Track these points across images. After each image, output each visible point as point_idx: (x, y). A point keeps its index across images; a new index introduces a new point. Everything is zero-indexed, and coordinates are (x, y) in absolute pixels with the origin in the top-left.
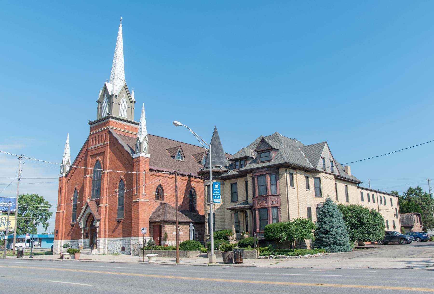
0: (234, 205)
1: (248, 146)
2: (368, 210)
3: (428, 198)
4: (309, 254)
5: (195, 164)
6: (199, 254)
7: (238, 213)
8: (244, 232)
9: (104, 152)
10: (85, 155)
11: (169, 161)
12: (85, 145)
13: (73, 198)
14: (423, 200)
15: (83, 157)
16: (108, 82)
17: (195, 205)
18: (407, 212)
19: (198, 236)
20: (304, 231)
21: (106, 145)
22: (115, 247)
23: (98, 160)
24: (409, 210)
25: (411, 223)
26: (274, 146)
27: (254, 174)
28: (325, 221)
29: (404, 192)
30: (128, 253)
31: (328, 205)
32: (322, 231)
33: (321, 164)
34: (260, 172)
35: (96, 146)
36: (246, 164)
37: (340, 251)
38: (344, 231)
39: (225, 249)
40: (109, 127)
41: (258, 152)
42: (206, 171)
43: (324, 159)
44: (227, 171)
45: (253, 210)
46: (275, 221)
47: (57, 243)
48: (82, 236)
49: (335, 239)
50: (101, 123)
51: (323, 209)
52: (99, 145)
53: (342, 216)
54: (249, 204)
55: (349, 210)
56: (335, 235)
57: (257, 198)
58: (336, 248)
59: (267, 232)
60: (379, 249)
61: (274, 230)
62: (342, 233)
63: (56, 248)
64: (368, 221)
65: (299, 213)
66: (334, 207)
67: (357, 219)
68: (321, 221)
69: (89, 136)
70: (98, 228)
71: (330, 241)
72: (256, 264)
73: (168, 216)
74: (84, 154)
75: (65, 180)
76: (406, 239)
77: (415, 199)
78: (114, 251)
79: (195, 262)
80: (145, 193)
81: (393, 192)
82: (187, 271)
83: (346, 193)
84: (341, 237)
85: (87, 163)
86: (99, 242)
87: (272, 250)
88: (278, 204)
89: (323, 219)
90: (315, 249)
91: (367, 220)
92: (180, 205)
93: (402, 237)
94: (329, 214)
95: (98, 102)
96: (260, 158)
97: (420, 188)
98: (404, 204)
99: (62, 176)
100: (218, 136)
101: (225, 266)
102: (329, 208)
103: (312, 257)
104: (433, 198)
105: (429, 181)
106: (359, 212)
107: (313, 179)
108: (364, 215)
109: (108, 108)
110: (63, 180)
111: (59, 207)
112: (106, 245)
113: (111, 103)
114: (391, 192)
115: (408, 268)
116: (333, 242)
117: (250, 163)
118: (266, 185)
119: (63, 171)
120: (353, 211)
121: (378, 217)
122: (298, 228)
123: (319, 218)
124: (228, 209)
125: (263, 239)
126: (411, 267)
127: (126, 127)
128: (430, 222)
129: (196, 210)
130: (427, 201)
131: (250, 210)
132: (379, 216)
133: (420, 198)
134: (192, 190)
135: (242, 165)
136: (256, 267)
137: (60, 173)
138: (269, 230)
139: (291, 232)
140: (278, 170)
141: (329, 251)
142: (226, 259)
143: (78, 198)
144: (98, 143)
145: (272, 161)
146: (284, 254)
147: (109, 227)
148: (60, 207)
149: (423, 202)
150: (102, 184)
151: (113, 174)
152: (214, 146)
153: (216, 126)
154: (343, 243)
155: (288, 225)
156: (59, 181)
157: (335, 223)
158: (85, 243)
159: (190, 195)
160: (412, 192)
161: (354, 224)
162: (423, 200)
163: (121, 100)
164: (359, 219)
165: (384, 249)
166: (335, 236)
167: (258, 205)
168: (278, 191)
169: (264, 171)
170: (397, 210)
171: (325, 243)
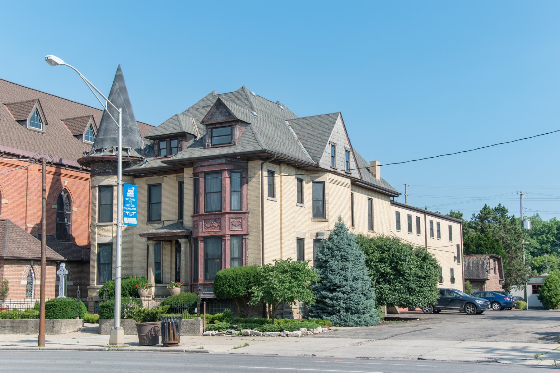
0: (153, 228)
1: (185, 111)
2: (411, 248)
3: (516, 228)
4: (303, 329)
5: (70, 140)
6: (81, 326)
7: (160, 243)
8: (173, 283)
11: (14, 130)
14: (508, 232)
17: (69, 225)
18: (477, 253)
19: (80, 290)
20: (295, 284)
24: (481, 249)
25: (483, 273)
26: (240, 117)
27: (198, 168)
28: (331, 267)
29: (474, 215)
31: (340, 235)
32: (325, 285)
33: (328, 155)
34: (210, 165)
36: (181, 149)
37: (357, 323)
38: (366, 286)
39: (144, 317)
41: (207, 125)
42: (97, 157)
43: (335, 146)
44: (141, 160)
45: (192, 241)
46: (236, 264)
49: (349, 300)
51: (331, 245)
53: (364, 257)
54: (184, 228)
55: (376, 246)
56: (349, 293)
57: (202, 217)
58: (350, 318)
59: (221, 285)
60: (428, 322)
61: (233, 280)
62: (363, 291)
64: (411, 269)
65: (281, 249)
66: (350, 240)
67: (390, 265)
68: (324, 267)
71: (339, 305)
72: (206, 348)
76: (475, 305)
77: (492, 229)
79: (78, 342)
81: (452, 214)
82: (79, 362)
83: (370, 214)
84: (360, 298)
87: (230, 320)
88: (244, 229)
89: (329, 262)
90: (310, 318)
91: (409, 268)
92: (37, 224)
93: (468, 301)
94: (340, 253)
96: (212, 137)
97: (503, 207)
98: (472, 238)
100: (125, 85)
101: (145, 350)
102: (341, 241)
103: (307, 335)
104: (526, 228)
105: (522, 195)
106: (395, 251)
107: (311, 183)
108: (403, 257)
114: (449, 214)
115: (489, 362)
116: (344, 306)
117: (191, 146)
118: (221, 192)
120: (384, 250)
121: (429, 262)
122: (285, 279)
123: (321, 260)
124: (141, 235)
125: (211, 297)
126: (496, 359)
128: (518, 272)
129: (71, 235)
130: (515, 233)
131: (186, 240)
132: (431, 260)
133: (503, 227)
134: (63, 193)
135: (173, 149)
136: (207, 352)
138: (225, 280)
139: (271, 285)
140: (246, 164)
141: (337, 323)
142: (145, 337)
145: (235, 145)
146: (255, 329)
149: (506, 235)
153: (119, 65)
154: (364, 309)
155: (263, 272)
157: (350, 270)
159: (57, 204)
160: (488, 216)
161: (384, 273)
162: (508, 231)
164: (394, 264)
165: (436, 322)
166: (349, 296)
167: (203, 231)
168: (244, 204)
169: (219, 164)
170: (460, 249)
171: (330, 309)
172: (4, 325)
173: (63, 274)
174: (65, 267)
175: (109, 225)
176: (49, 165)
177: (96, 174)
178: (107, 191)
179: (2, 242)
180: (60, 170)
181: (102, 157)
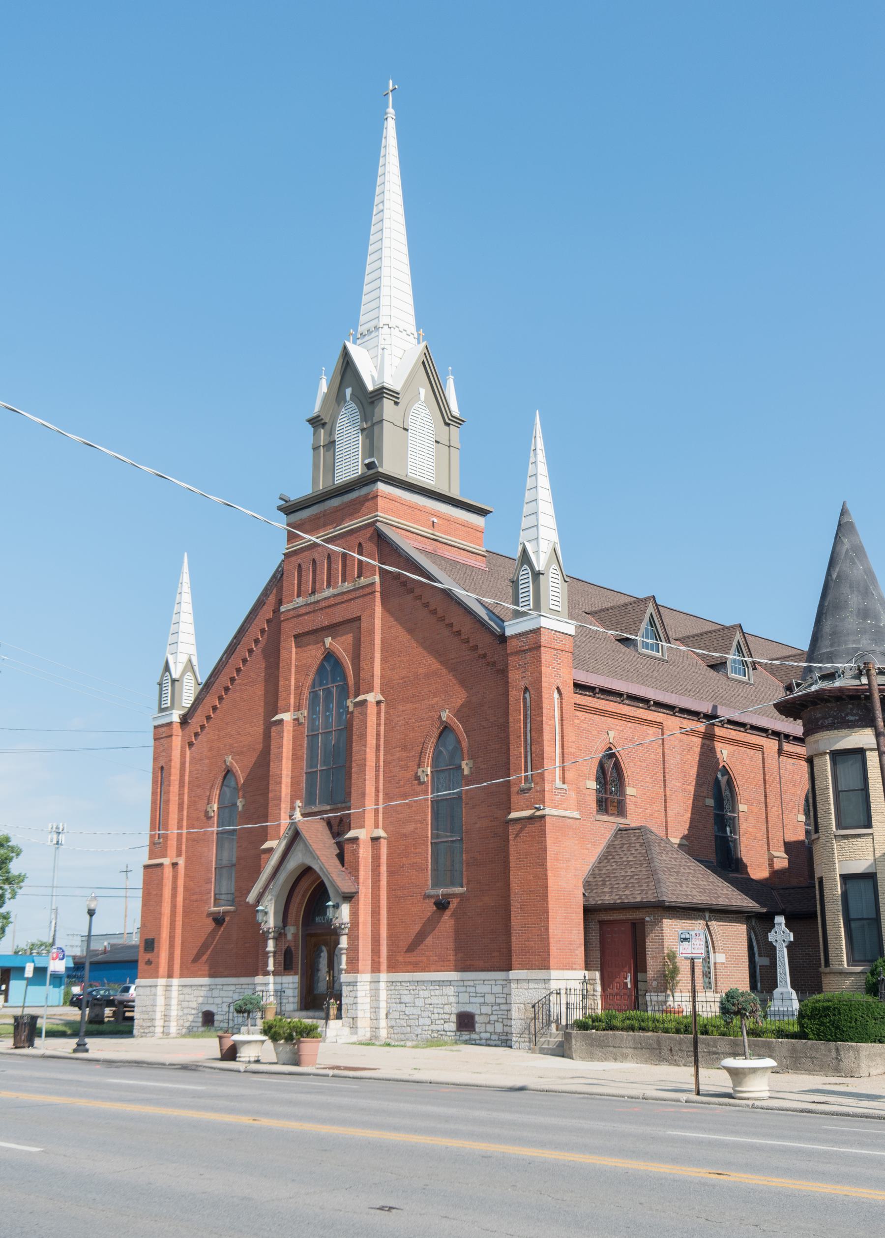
9: (358, 619)
10: (265, 636)
12: (266, 593)
13: (215, 807)
15: (257, 641)
16: (354, 343)
21: (367, 591)
22: (424, 1014)
23: (330, 656)
30: (490, 1039)
35: (318, 597)
40: (377, 516)
42: (830, 690)
47: (153, 989)
48: (271, 961)
50: (335, 502)
52: (331, 591)
63: (147, 1012)
69: (283, 557)
70: (347, 931)
73: (668, 884)
74: (263, 631)
75: (180, 738)
78: (419, 1031)
80: (564, 783)
85: (281, 665)
86: (350, 988)
95: (316, 422)
99: (166, 720)
109: (360, 445)
110: (171, 736)
111: (154, 844)
112: (383, 1004)
113: (373, 425)
119: (169, 701)
127: (436, 521)
137: (157, 709)
143: (240, 808)
144: (325, 584)
147: (390, 926)
148: (160, 843)
150: (355, 747)
151: (401, 708)
152: (851, 587)
156: (155, 740)
158: (279, 993)
163: (413, 410)
172: (714, 1049)
173: (784, 941)
174: (786, 926)
175: (864, 835)
176: (696, 719)
177: (819, 728)
178: (850, 762)
179: (650, 872)
180: (714, 729)
181: (841, 690)
